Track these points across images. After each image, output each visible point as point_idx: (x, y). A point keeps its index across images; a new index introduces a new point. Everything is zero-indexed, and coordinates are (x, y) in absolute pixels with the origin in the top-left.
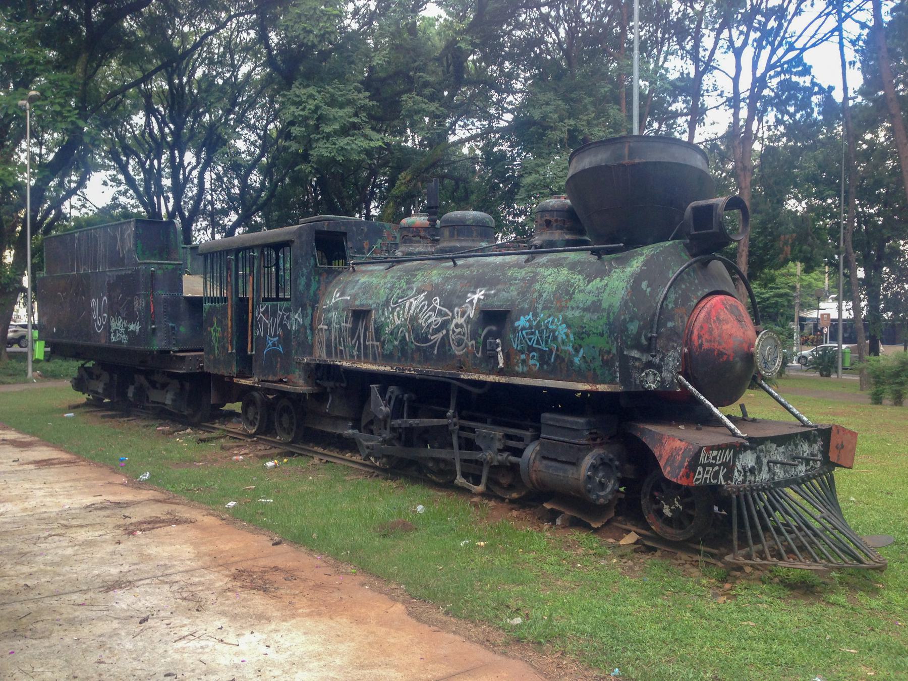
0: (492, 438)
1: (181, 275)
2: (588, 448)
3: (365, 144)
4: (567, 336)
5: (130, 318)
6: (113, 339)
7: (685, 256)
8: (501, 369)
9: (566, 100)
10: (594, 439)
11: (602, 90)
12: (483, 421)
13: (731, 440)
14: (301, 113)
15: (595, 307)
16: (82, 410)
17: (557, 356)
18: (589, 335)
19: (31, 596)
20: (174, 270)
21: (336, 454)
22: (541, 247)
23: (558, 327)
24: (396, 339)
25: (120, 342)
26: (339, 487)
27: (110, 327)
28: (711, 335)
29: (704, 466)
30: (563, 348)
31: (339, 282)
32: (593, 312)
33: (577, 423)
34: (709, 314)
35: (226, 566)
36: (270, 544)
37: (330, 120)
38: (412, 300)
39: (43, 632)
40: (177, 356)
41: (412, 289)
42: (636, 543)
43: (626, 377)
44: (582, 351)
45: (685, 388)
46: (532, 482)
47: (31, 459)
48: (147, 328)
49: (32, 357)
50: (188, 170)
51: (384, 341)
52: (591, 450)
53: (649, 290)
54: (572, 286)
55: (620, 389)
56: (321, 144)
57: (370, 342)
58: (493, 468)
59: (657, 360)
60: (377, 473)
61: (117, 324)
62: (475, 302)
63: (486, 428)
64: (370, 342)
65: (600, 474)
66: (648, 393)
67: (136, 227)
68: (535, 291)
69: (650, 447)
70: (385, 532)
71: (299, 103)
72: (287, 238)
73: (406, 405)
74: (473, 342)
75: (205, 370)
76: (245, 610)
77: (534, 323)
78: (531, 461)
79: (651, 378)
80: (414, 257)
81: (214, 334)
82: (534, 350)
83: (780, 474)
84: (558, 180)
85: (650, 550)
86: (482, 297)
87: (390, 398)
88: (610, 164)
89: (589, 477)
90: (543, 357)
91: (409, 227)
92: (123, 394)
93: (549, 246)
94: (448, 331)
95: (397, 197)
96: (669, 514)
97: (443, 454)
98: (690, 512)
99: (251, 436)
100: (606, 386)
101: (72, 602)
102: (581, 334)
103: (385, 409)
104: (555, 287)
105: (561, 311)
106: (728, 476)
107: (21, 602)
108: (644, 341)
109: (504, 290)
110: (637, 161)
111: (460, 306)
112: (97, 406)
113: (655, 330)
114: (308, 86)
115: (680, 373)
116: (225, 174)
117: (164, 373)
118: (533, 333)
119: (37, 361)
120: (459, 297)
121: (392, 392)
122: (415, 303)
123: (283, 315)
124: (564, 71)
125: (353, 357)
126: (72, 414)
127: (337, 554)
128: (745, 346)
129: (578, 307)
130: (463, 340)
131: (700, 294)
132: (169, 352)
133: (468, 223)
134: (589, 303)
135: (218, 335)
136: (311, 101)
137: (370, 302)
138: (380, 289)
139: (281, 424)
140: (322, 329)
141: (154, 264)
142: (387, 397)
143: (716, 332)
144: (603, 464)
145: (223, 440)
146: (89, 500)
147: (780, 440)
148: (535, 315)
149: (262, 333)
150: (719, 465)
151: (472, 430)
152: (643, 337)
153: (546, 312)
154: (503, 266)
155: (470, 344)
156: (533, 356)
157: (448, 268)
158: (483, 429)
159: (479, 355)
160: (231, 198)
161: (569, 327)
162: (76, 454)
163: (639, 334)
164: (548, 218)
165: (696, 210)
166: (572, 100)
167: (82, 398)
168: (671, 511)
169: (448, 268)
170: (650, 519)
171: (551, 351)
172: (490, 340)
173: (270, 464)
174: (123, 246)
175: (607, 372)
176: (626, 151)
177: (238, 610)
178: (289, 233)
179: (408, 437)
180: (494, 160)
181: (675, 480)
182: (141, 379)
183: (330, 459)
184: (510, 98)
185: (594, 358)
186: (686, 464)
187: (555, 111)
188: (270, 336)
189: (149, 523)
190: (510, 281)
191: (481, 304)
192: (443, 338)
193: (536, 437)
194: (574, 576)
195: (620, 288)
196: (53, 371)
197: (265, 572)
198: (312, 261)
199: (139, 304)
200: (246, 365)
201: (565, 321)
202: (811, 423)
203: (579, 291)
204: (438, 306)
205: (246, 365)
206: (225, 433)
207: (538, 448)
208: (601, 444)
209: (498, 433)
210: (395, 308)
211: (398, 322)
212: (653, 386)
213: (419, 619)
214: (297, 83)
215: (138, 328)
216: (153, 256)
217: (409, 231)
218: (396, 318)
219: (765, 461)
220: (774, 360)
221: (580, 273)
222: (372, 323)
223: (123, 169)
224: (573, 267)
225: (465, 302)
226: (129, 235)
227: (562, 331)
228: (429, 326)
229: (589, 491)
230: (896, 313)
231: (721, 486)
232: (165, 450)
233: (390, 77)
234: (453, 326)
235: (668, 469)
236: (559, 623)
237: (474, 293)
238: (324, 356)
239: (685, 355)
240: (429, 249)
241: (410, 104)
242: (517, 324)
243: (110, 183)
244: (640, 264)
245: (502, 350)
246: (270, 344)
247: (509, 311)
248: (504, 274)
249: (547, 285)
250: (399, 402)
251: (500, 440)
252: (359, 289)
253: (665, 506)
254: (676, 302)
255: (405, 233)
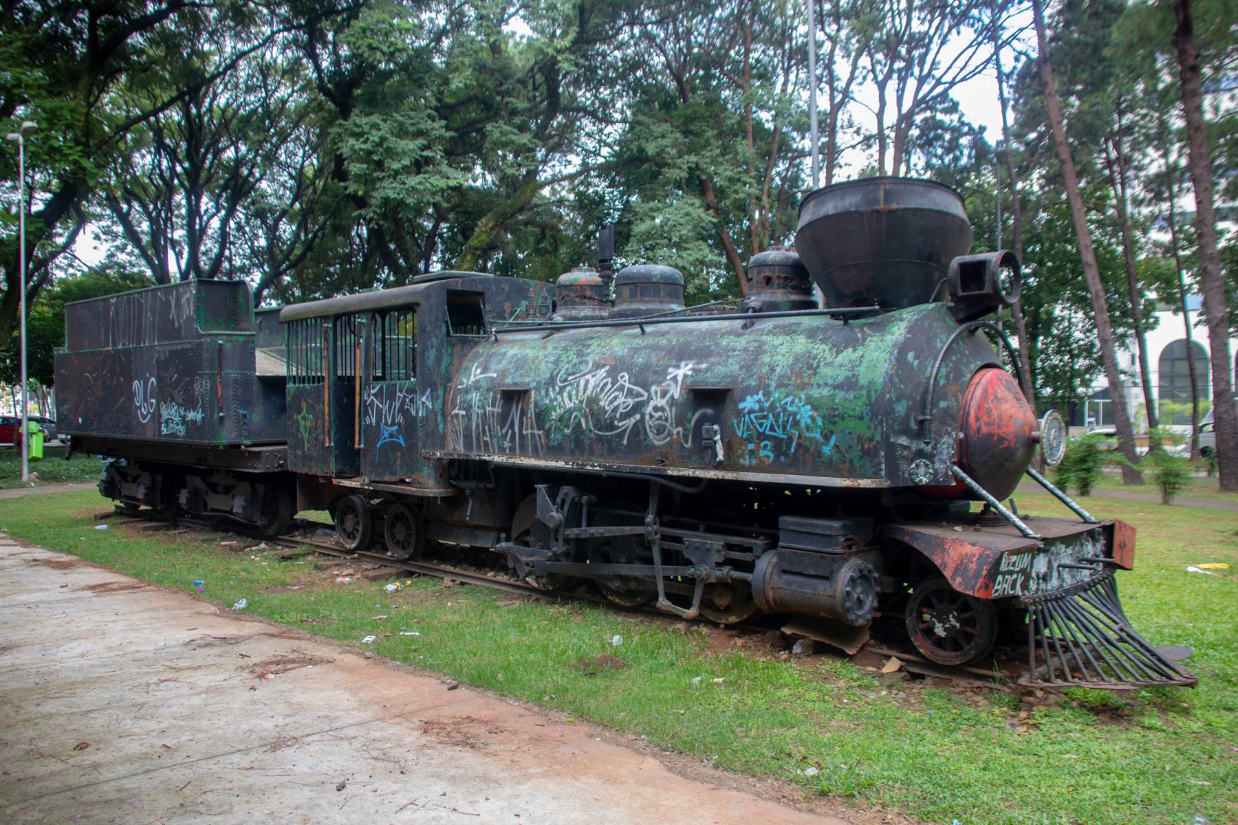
0: (708, 549)
1: (254, 349)
2: (844, 558)
3: (442, 183)
4: (813, 419)
5: (189, 404)
6: (164, 431)
7: (950, 322)
8: (721, 462)
9: (686, 133)
10: (850, 547)
11: (729, 122)
12: (695, 528)
13: (1026, 542)
14: (363, 146)
15: (850, 384)
16: (113, 520)
17: (799, 445)
18: (843, 419)
19: (180, 760)
20: (246, 342)
21: (472, 574)
22: (760, 310)
23: (799, 408)
24: (567, 426)
25: (174, 435)
26: (492, 615)
27: (160, 416)
28: (989, 417)
29: (1004, 574)
30: (808, 434)
31: (477, 355)
32: (848, 390)
33: (830, 528)
34: (985, 391)
35: (404, 716)
36: (445, 687)
37: (397, 154)
38: (588, 377)
39: (221, 806)
40: (250, 452)
41: (587, 362)
42: (900, 670)
43: (893, 471)
44: (833, 439)
45: (960, 481)
46: (768, 602)
47: (83, 584)
48: (212, 416)
49: (28, 453)
50: (205, 218)
51: (550, 429)
52: (847, 560)
53: (916, 363)
54: (814, 358)
55: (886, 484)
56: (386, 184)
57: (529, 431)
58: (709, 587)
59: (928, 449)
60: (534, 596)
61: (170, 412)
62: (680, 378)
63: (697, 537)
64: (529, 431)
65: (859, 590)
66: (917, 489)
67: (198, 290)
68: (763, 365)
69: (926, 554)
70: (590, 670)
71: (361, 135)
72: (410, 300)
73: (585, 509)
74: (680, 429)
75: (290, 468)
76: (461, 771)
77: (767, 405)
78: (768, 576)
79: (922, 470)
80: (582, 323)
81: (302, 423)
82: (767, 438)
83: (1068, 581)
84: (679, 228)
85: (915, 677)
86: (690, 373)
87: (563, 501)
88: (862, 209)
89: (848, 593)
90: (780, 447)
91: (571, 285)
92: (171, 499)
93: (770, 309)
94: (643, 416)
95: (476, 249)
96: (943, 634)
97: (637, 570)
98: (970, 630)
99: (352, 552)
100: (869, 481)
101: (236, 766)
102: (832, 417)
103: (557, 516)
104: (791, 359)
105: (803, 389)
106: (1025, 586)
107: (171, 767)
108: (914, 426)
109: (719, 363)
110: (894, 206)
111: (659, 384)
112: (129, 516)
113: (928, 411)
114: (371, 114)
115: (954, 463)
116: (248, 223)
117: (227, 473)
118: (765, 417)
119: (35, 460)
120: (655, 373)
121: (566, 494)
122: (593, 381)
123: (405, 397)
124: (673, 99)
125: (504, 450)
126: (105, 526)
127: (540, 699)
128: (1026, 429)
129: (826, 384)
130: (665, 427)
131: (973, 367)
132: (239, 446)
133: (654, 280)
134: (840, 379)
135: (308, 424)
136: (374, 132)
137: (527, 380)
138: (539, 363)
139: (393, 536)
140: (457, 415)
141: (221, 336)
142: (559, 500)
143: (995, 413)
144: (862, 577)
145: (310, 558)
146: (186, 636)
147: (1068, 540)
148: (767, 394)
149: (374, 421)
150: (1017, 572)
151: (678, 540)
152: (912, 421)
153: (783, 390)
154: (712, 333)
155: (675, 432)
156: (766, 446)
157: (635, 336)
158: (693, 539)
159: (689, 445)
160: (255, 252)
161: (815, 408)
162: (136, 576)
163: (907, 417)
164: (768, 274)
165: (963, 266)
166: (691, 132)
167: (110, 505)
168: (945, 630)
169: (635, 336)
170: (918, 641)
171: (790, 439)
172: (706, 426)
173: (391, 587)
174: (179, 315)
175: (868, 464)
176: (881, 194)
177: (453, 772)
178: (414, 293)
179: (580, 549)
180: (589, 206)
181: (971, 593)
182: (198, 482)
183: (464, 580)
184: (609, 129)
185: (850, 447)
186: (984, 573)
187: (673, 146)
188: (386, 424)
189: (278, 663)
190: (728, 351)
191: (689, 381)
192: (635, 424)
193: (773, 544)
194: (848, 714)
195: (882, 360)
196: (50, 472)
197: (459, 723)
198: (444, 330)
199: (201, 387)
200: (350, 460)
201: (809, 401)
202: (1093, 519)
203: (826, 365)
204: (627, 385)
205: (350, 460)
206: (313, 549)
207: (775, 560)
208: (857, 553)
209: (717, 542)
210: (565, 387)
211: (569, 405)
212: (925, 480)
213: (685, 776)
214: (356, 111)
215: (199, 416)
216: (218, 326)
217: (571, 290)
218: (566, 400)
219: (1055, 565)
220: (1058, 446)
221: (823, 341)
222: (532, 406)
223: (124, 219)
224: (811, 334)
225: (665, 379)
226: (188, 300)
227: (805, 414)
228: (615, 409)
229: (848, 610)
230: (1056, 389)
231: (1017, 597)
232: (244, 570)
233: (462, 103)
234: (649, 409)
235: (959, 580)
236: (864, 771)
237: (678, 367)
238: (461, 449)
239: (961, 441)
240: (597, 313)
241: (496, 135)
242: (741, 406)
243: (103, 237)
244: (903, 331)
245: (722, 439)
246: (386, 434)
247: (729, 390)
248: (717, 344)
249: (780, 357)
250: (576, 507)
251: (719, 551)
252: (510, 363)
253: (937, 624)
254: (947, 377)
255: (565, 293)
